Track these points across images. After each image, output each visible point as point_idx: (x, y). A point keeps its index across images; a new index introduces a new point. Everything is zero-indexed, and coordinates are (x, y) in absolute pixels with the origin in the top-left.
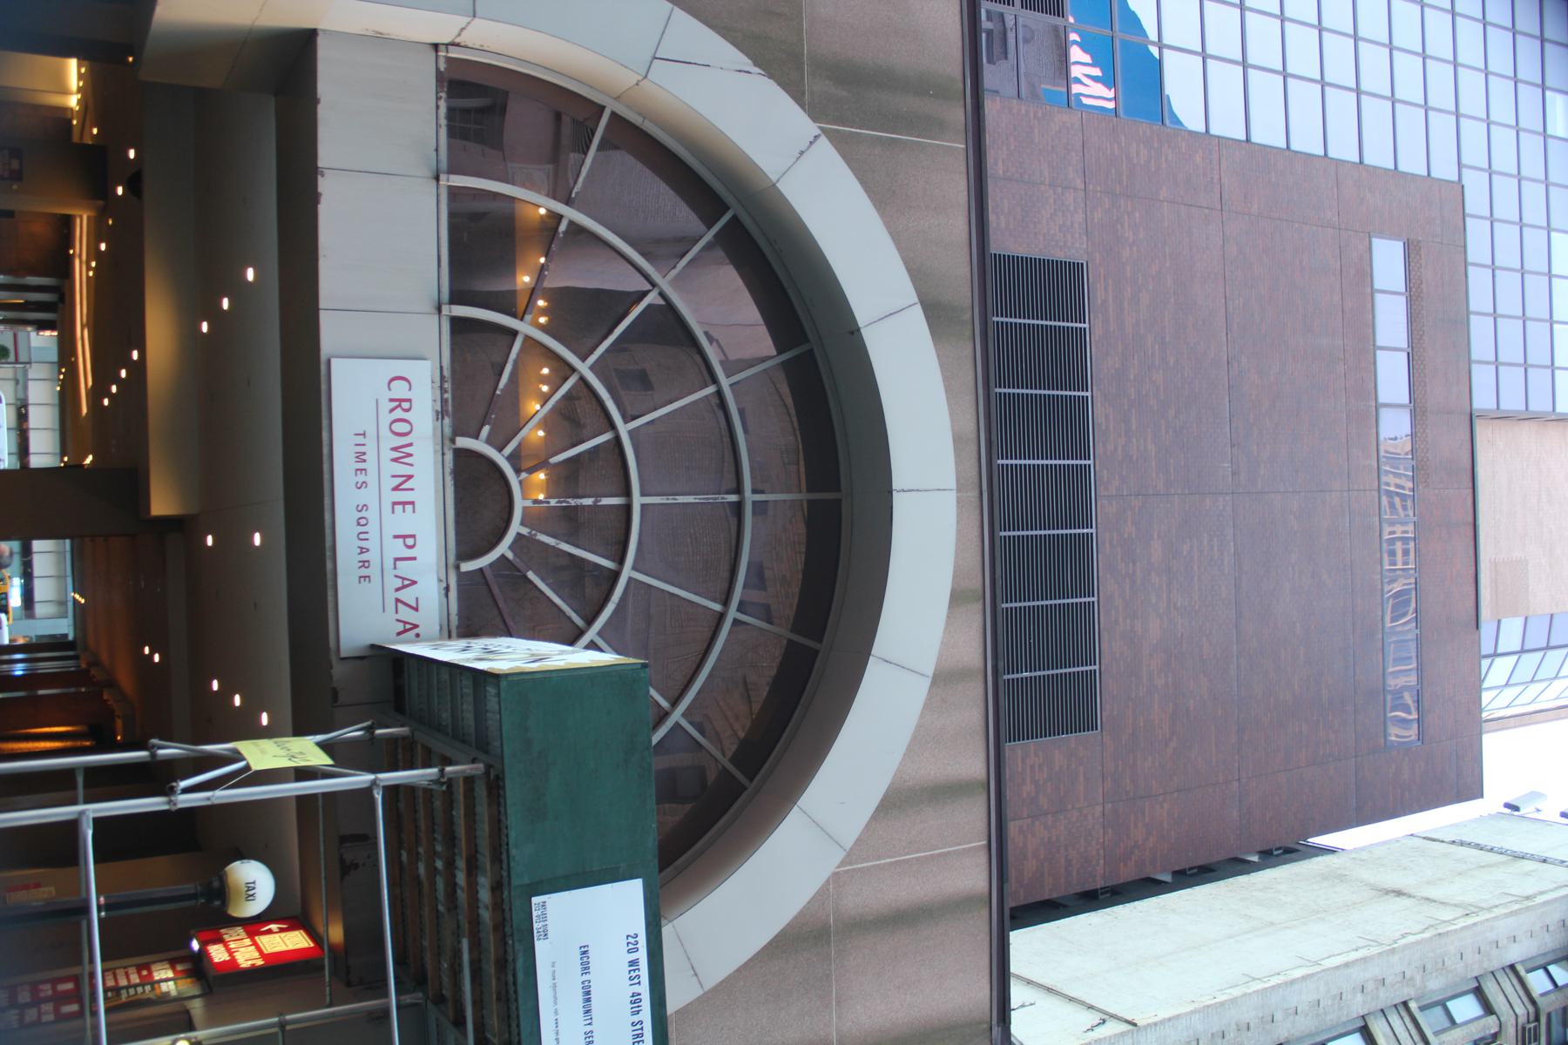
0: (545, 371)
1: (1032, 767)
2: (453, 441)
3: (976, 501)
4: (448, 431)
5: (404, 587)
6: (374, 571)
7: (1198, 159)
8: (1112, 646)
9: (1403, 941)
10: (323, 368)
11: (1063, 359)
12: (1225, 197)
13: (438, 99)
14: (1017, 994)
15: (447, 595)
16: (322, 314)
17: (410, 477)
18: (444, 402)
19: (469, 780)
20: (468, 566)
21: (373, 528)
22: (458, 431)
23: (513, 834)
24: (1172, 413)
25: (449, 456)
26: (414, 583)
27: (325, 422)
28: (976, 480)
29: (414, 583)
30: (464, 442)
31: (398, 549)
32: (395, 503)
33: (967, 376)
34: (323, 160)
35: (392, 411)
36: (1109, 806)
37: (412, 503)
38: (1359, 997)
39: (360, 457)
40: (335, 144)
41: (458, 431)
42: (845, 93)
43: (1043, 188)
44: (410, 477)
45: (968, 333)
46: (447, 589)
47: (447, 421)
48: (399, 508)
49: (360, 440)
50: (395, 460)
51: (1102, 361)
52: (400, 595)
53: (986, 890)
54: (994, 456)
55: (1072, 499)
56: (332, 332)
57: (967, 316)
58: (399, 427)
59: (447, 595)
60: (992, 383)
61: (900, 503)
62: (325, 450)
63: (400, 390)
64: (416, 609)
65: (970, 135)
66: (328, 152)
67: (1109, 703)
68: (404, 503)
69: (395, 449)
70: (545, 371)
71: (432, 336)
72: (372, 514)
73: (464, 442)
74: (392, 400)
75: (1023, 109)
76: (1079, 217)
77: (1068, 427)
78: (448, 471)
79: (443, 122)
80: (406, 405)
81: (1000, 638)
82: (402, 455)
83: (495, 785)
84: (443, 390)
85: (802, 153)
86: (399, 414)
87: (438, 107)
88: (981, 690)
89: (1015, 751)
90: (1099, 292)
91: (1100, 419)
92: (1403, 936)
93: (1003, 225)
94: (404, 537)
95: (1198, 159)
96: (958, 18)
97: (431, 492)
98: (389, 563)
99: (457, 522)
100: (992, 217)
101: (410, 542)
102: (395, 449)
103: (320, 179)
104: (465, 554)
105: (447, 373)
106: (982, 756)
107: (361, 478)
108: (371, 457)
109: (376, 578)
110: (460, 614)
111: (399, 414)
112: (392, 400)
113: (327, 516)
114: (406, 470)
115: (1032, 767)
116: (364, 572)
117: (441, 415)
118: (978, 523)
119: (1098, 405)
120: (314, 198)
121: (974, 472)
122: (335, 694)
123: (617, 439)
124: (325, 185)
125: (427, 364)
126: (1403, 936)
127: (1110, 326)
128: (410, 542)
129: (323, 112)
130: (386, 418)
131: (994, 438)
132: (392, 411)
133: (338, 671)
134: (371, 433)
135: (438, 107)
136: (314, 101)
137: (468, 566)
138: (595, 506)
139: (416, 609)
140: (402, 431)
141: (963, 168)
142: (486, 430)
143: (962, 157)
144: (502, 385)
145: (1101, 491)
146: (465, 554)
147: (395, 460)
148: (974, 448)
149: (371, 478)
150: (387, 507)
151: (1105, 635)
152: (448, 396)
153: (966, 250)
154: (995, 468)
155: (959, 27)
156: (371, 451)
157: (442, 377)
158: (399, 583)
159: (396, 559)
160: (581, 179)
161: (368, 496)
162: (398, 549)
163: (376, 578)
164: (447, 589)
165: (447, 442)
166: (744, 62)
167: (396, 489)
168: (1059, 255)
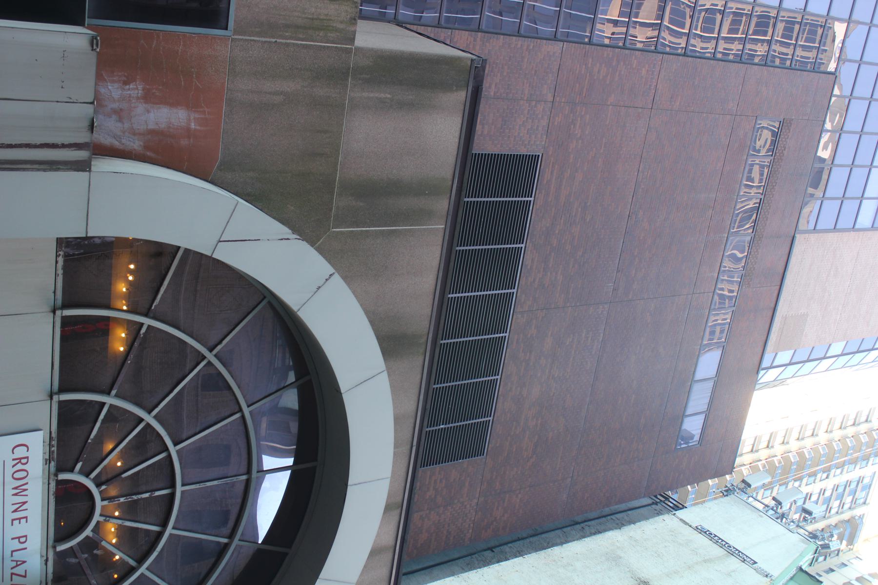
0: (132, 267)
1: (435, 481)
2: (54, 547)
3: (407, 452)
4: (53, 469)
5: (17, 566)
7: (644, 72)
8: (504, 405)
11: (511, 223)
12: (657, 98)
13: (57, 256)
15: (46, 564)
18: (51, 453)
20: (60, 548)
22: (60, 469)
24: (580, 253)
25: (53, 484)
26: (24, 562)
29: (24, 562)
30: (63, 476)
31: (16, 545)
32: (13, 520)
33: (411, 404)
35: (13, 466)
36: (482, 499)
37: (26, 518)
41: (60, 469)
42: (361, 204)
43: (522, 102)
44: (24, 503)
45: (422, 350)
46: (47, 560)
47: (53, 464)
50: (16, 494)
51: (538, 222)
52: (14, 571)
54: (463, 193)
57: (423, 340)
59: (46, 564)
60: (440, 336)
61: (350, 490)
63: (21, 452)
64: (25, 576)
65: (450, 218)
67: (492, 443)
68: (20, 519)
71: (45, 415)
73: (63, 476)
74: (14, 460)
75: (520, 43)
76: (544, 123)
77: (505, 268)
78: (51, 493)
79: (60, 272)
80: (24, 461)
82: (20, 491)
84: (50, 446)
86: (19, 467)
87: (57, 262)
89: (425, 473)
90: (546, 175)
91: (528, 262)
93: (486, 132)
94: (19, 538)
95: (644, 72)
100: (478, 127)
101: (23, 540)
104: (60, 538)
105: (54, 435)
111: (19, 467)
112: (14, 460)
115: (435, 481)
117: (48, 461)
119: (528, 252)
121: (409, 435)
125: (41, 433)
127: (547, 205)
128: (23, 540)
130: (9, 471)
131: (428, 407)
132: (13, 466)
135: (57, 262)
137: (60, 548)
138: (150, 497)
139: (25, 576)
143: (441, 235)
144: (92, 436)
145: (518, 309)
146: (60, 538)
147: (16, 494)
148: (412, 421)
151: (501, 398)
152: (54, 449)
153: (431, 297)
154: (462, 203)
155: (457, 140)
157: (51, 438)
159: (12, 552)
160: (159, 296)
162: (16, 545)
164: (47, 560)
165: (52, 477)
166: (285, 231)
168: (523, 151)
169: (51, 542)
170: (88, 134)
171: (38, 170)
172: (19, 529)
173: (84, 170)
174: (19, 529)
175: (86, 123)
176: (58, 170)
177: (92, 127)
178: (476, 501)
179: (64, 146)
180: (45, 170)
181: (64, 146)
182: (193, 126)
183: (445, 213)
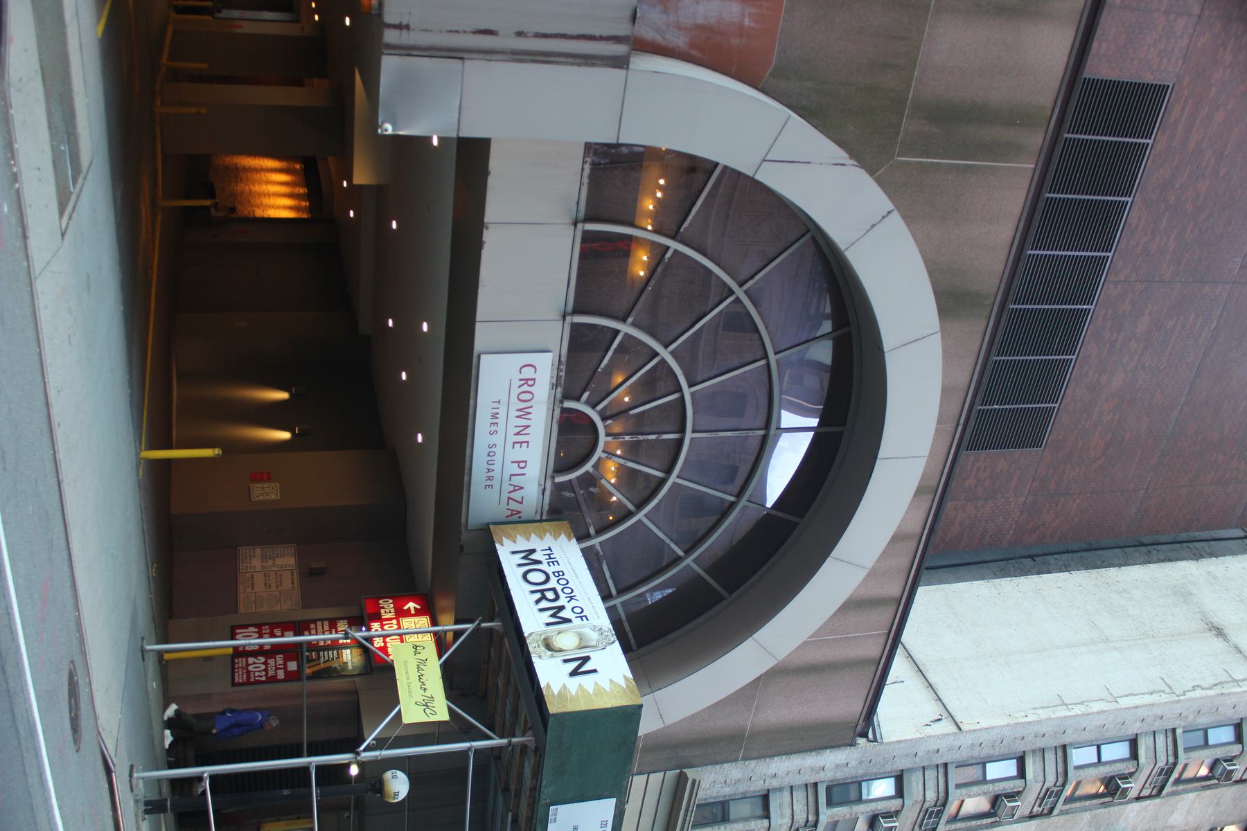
0: (662, 182)
1: (978, 469)
3: (952, 430)
4: (559, 396)
6: (496, 482)
8: (1075, 392)
9: (1189, 695)
10: (475, 360)
11: (1118, 169)
13: (584, 163)
14: (899, 666)
16: (478, 326)
17: (527, 427)
18: (558, 377)
19: (524, 747)
20: (559, 479)
21: (498, 458)
22: (566, 396)
23: (544, 782)
25: (558, 411)
27: (472, 394)
28: (965, 387)
30: (569, 404)
33: (964, 375)
34: (490, 215)
36: (1030, 498)
38: (1138, 724)
39: (495, 416)
40: (499, 204)
41: (566, 396)
42: (936, 130)
44: (527, 427)
45: (986, 313)
46: (544, 490)
47: (559, 389)
48: (517, 446)
49: (496, 405)
50: (519, 417)
52: (512, 495)
53: (899, 594)
55: (1084, 282)
56: (483, 336)
57: (989, 302)
58: (523, 397)
62: (471, 411)
63: (528, 373)
65: (1043, 156)
66: (492, 213)
67: (1054, 433)
68: (521, 443)
69: (520, 410)
70: (662, 182)
71: (556, 336)
72: (499, 450)
73: (569, 404)
76: (1183, 43)
77: (1101, 225)
79: (586, 181)
80: (530, 382)
81: (1013, 287)
82: (524, 413)
83: (539, 751)
84: (559, 370)
85: (873, 226)
86: (525, 388)
88: (977, 346)
91: (1133, 220)
92: (1194, 688)
93: (1102, 52)
96: (1067, 52)
97: (541, 445)
98: (506, 477)
99: (578, 282)
100: (1095, 45)
101: (522, 465)
102: (520, 410)
103: (485, 233)
104: (560, 469)
105: (564, 359)
106: (901, 584)
107: (494, 428)
108: (502, 415)
109: (496, 487)
110: (550, 504)
111: (525, 388)
113: (468, 450)
115: (978, 469)
116: (489, 483)
117: (555, 386)
118: (948, 444)
120: (479, 245)
122: (462, 548)
123: (682, 399)
124: (487, 236)
125: (550, 355)
126: (1194, 688)
128: (522, 465)
129: (491, 181)
130: (515, 391)
133: (465, 536)
134: (504, 400)
136: (485, 173)
137: (559, 479)
141: (1026, 186)
142: (586, 395)
144: (603, 365)
145: (1112, 278)
146: (560, 469)
147: (519, 417)
148: (962, 395)
149: (501, 429)
150: (509, 444)
153: (1006, 251)
158: (512, 488)
161: (498, 439)
163: (496, 487)
164: (544, 490)
165: (557, 403)
166: (840, 154)
167: (517, 434)
168: (1148, 78)
169: (550, 472)
170: (629, 26)
171: (572, 64)
172: (519, 453)
173: (621, 67)
174: (519, 453)
175: (628, 14)
176: (593, 65)
177: (634, 18)
178: (1023, 499)
179: (602, 38)
180: (579, 65)
181: (602, 38)
182: (747, 22)
183: (1037, 150)
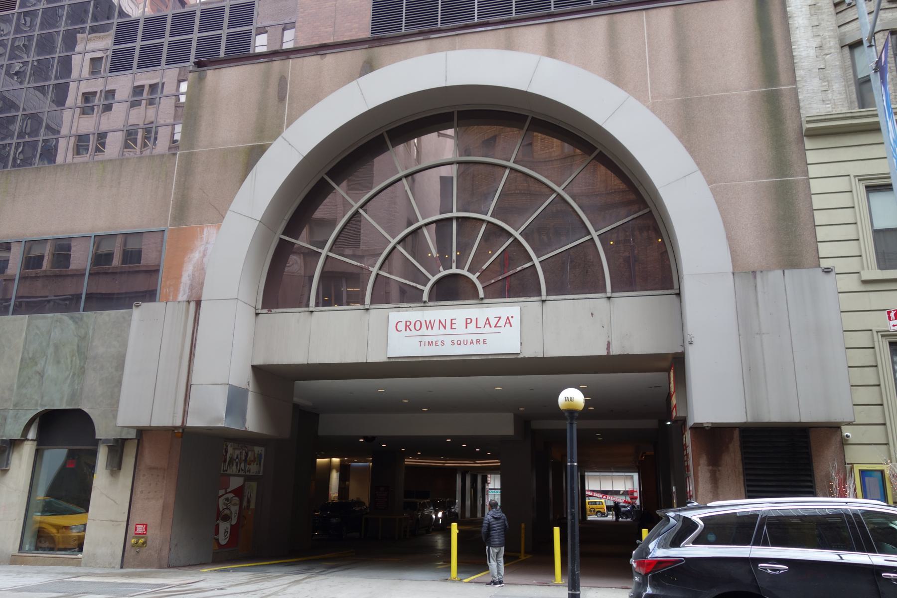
17: (440, 321)
39: (430, 344)
44: (440, 321)
49: (423, 344)
63: (401, 326)
68: (452, 324)
71: (378, 313)
73: (425, 297)
80: (408, 324)
82: (430, 325)
86: (412, 327)
101: (469, 321)
104: (474, 295)
107: (439, 343)
111: (412, 327)
114: (437, 323)
116: (482, 342)
128: (469, 321)
130: (414, 332)
140: (420, 325)
149: (440, 339)
156: (427, 339)
167: (445, 327)
172: (460, 324)
174: (460, 324)
